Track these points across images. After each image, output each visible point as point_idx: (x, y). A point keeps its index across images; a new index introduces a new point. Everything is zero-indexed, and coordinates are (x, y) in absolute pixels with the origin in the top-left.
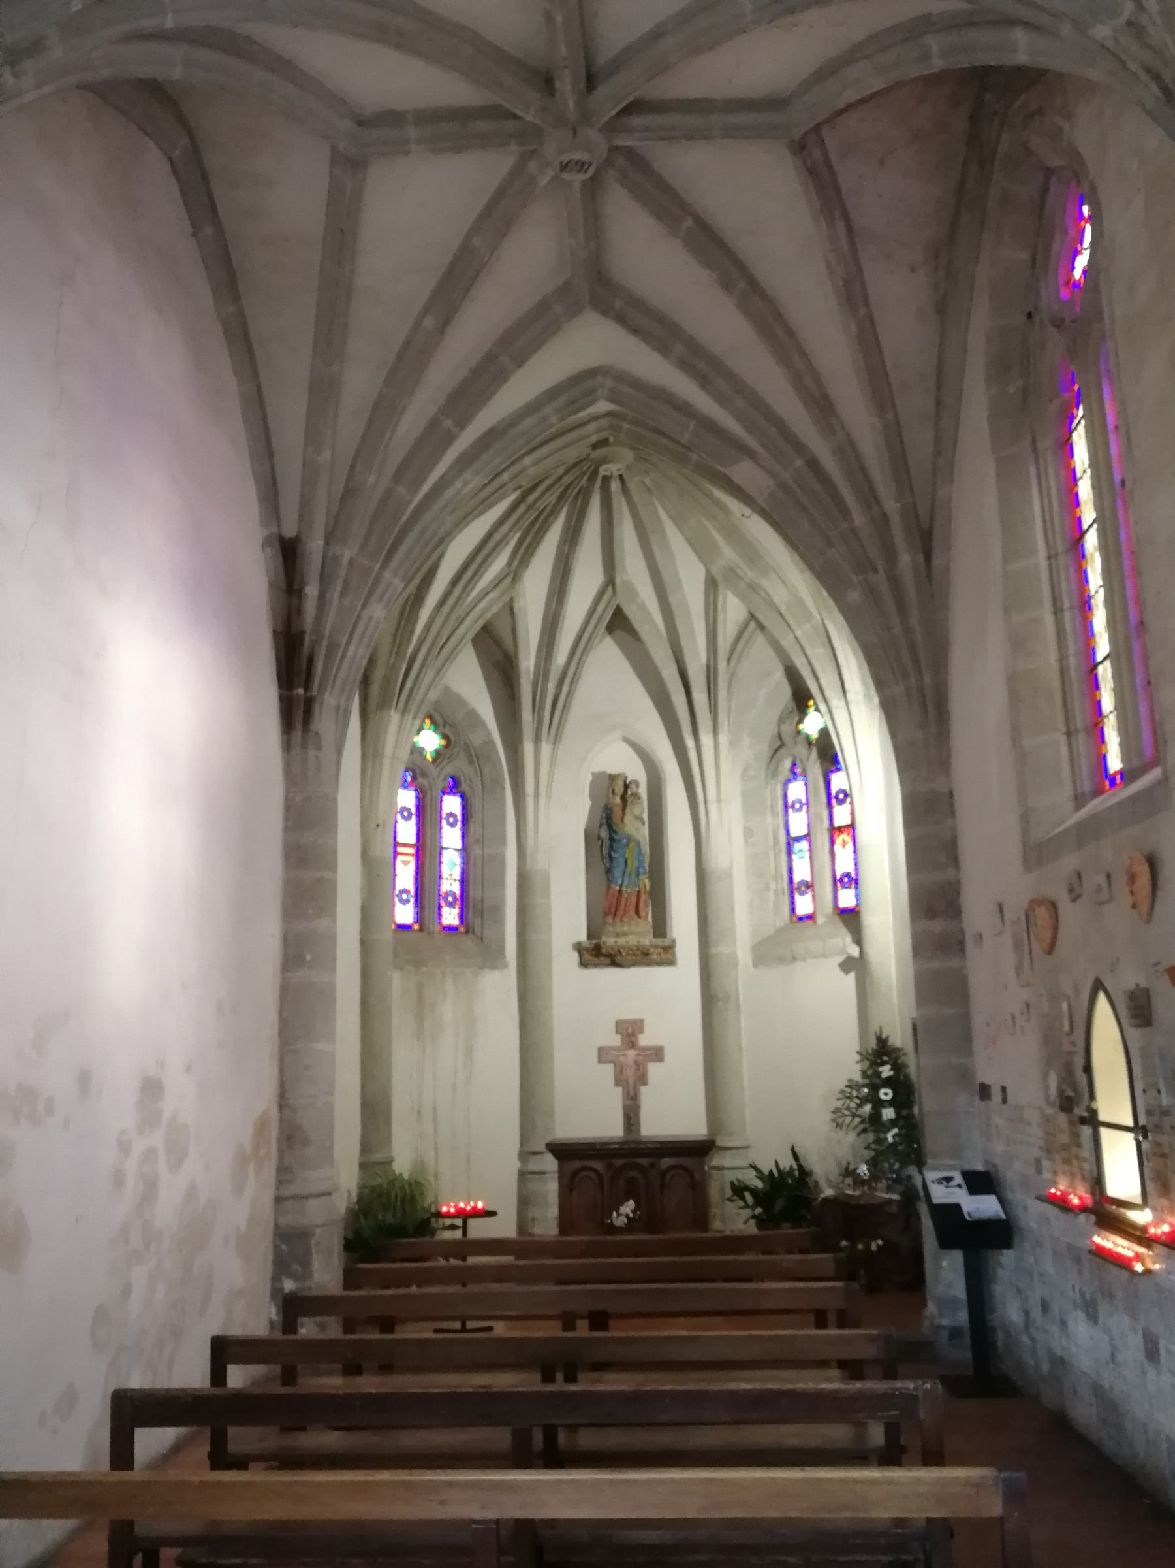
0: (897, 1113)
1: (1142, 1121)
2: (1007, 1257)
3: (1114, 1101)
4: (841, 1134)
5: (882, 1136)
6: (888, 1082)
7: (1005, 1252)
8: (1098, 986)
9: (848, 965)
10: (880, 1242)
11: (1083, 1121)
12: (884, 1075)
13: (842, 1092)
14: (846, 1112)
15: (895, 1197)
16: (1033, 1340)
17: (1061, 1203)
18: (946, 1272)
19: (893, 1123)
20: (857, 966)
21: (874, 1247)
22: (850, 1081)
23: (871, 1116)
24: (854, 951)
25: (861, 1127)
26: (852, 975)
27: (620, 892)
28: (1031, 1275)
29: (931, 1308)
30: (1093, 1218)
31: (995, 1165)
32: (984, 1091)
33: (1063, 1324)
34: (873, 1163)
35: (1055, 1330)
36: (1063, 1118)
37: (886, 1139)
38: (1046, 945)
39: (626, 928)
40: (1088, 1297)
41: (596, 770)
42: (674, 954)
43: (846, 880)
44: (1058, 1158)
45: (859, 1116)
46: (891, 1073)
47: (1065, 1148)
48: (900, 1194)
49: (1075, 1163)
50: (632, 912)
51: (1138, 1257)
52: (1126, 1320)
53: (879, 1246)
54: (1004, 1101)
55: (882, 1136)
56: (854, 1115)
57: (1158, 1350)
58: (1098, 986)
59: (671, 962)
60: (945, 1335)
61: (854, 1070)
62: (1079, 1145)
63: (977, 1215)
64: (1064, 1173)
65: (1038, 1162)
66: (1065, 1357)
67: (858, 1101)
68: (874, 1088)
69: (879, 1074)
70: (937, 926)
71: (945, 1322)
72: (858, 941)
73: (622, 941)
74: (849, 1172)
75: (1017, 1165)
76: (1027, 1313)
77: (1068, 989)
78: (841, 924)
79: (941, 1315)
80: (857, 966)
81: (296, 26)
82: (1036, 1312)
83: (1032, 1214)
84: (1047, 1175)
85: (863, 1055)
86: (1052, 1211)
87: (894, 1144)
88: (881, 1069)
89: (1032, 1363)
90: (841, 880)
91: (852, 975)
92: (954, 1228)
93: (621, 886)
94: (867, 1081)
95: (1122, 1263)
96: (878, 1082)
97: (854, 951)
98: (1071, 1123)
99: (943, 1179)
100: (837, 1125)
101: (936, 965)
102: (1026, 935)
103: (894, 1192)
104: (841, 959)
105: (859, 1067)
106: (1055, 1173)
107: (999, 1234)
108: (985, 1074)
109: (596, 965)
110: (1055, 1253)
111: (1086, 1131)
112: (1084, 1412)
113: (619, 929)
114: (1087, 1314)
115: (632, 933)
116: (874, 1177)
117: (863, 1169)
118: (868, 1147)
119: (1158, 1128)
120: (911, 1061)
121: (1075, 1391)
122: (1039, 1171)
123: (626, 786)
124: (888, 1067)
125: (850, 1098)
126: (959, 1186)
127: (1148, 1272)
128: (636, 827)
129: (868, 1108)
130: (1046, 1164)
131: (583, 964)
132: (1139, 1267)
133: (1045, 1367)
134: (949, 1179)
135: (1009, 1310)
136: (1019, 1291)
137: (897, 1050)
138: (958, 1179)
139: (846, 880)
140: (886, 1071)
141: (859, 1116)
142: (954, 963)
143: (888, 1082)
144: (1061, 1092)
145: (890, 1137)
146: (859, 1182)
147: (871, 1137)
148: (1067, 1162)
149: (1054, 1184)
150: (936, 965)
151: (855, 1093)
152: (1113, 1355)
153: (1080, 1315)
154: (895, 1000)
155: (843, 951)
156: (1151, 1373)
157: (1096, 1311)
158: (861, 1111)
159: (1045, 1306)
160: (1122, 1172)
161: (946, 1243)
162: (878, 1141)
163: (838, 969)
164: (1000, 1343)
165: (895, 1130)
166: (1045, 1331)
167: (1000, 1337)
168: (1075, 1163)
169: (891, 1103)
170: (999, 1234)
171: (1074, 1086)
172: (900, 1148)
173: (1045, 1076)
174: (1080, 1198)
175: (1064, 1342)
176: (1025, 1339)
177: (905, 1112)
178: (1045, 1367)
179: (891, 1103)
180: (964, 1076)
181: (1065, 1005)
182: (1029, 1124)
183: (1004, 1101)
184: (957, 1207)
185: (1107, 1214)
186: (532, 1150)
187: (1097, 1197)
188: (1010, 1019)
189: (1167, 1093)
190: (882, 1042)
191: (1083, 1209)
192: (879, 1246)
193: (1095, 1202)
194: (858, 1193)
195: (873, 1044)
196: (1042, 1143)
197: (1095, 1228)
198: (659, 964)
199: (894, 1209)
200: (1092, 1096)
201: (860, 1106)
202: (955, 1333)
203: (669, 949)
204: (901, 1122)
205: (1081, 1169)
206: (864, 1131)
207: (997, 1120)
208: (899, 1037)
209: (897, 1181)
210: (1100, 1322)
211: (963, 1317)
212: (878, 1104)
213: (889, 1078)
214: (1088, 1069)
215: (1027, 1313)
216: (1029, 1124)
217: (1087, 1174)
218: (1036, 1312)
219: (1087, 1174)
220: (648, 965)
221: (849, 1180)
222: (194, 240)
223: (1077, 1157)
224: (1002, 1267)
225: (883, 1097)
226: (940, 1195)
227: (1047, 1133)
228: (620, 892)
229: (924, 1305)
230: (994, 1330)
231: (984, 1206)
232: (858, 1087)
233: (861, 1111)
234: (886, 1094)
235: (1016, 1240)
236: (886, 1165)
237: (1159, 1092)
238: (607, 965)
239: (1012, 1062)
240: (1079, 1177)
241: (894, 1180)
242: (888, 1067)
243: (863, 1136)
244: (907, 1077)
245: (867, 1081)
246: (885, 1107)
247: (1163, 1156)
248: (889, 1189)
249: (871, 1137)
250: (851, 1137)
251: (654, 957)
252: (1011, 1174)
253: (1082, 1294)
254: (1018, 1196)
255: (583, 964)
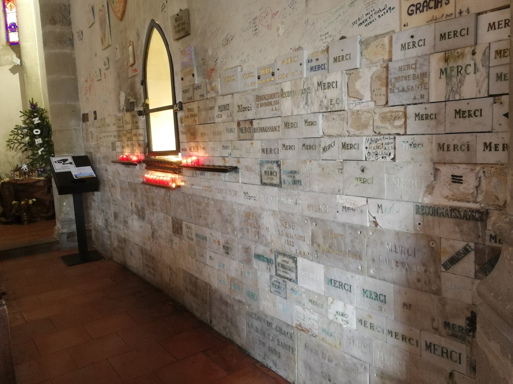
0: (43, 140)
1: (179, 99)
2: (97, 195)
3: (160, 92)
4: (13, 153)
5: (35, 152)
6: (38, 126)
7: (96, 193)
8: (153, 25)
9: (14, 70)
10: (34, 200)
11: (140, 113)
12: (35, 123)
13: (12, 131)
14: (16, 141)
15: (42, 178)
16: (110, 232)
17: (128, 163)
18: (65, 206)
19: (41, 145)
20: (19, 69)
21: (30, 202)
22: (16, 126)
23: (28, 143)
24: (18, 62)
25: (24, 149)
26: (17, 75)
28: (109, 202)
29: (58, 225)
30: (144, 165)
31: (90, 153)
32: (85, 118)
33: (126, 222)
34: (31, 165)
35: (121, 226)
36: (128, 116)
37: (38, 153)
38: (119, 15)
40: (139, 207)
43: (13, 27)
44: (124, 139)
45: (23, 143)
46: (39, 121)
47: (130, 131)
48: (45, 177)
49: (134, 138)
51: (173, 181)
52: (162, 215)
53: (33, 202)
54: (95, 118)
55: (35, 152)
56: (21, 143)
57: (181, 228)
58: (153, 25)
60: (65, 237)
61: (19, 121)
62: (137, 128)
63: (80, 176)
64: (128, 146)
65: (113, 144)
66: (126, 237)
67: (22, 136)
68: (31, 129)
69: (33, 123)
70: (58, 29)
71: (65, 231)
72: (19, 57)
74: (18, 169)
75: (103, 150)
76: (106, 220)
77: (132, 37)
78: (11, 50)
79: (62, 228)
80: (19, 69)
82: (111, 219)
83: (112, 172)
84: (119, 150)
85: (24, 113)
86: (120, 168)
87: (42, 155)
88: (34, 120)
89: (109, 243)
90: (10, 27)
91: (17, 75)
92: (69, 184)
94: (27, 126)
95: (163, 185)
96: (33, 126)
97: (18, 62)
98: (133, 116)
99: (62, 160)
100: (10, 148)
101: (57, 51)
102: (107, 15)
103: (42, 177)
104: (11, 66)
105: (23, 118)
106: (123, 147)
107: (93, 184)
108: (85, 108)
110: (122, 188)
111: (142, 118)
112: (135, 262)
114: (139, 216)
116: (31, 171)
117: (25, 167)
118: (28, 158)
119: (191, 100)
120: (49, 115)
121: (131, 253)
122: (114, 149)
124: (38, 118)
125: (18, 134)
126: (71, 163)
127: (178, 187)
129: (27, 139)
130: (118, 144)
132: (174, 185)
133: (116, 244)
134: (65, 161)
135: (97, 219)
136: (103, 211)
137: (43, 110)
138: (70, 160)
139: (13, 27)
140: (36, 121)
141: (23, 143)
142: (67, 51)
143: (38, 126)
144: (127, 100)
145: (40, 152)
146: (23, 173)
147: (30, 153)
148: (130, 139)
149: (122, 153)
150: (57, 51)
151: (20, 132)
152: (153, 233)
153: (135, 217)
154: (41, 87)
155: (12, 62)
156: (176, 240)
157: (144, 213)
158: (23, 140)
159: (116, 216)
160: (163, 133)
161: (62, 191)
162: (34, 155)
163: (10, 72)
164: (93, 237)
165: (43, 149)
166: (116, 227)
167: (93, 233)
168: (134, 138)
169: (40, 136)
170: (93, 184)
171: (135, 96)
172: (45, 157)
173: (119, 95)
174: (137, 156)
175: (126, 231)
176: (106, 233)
177: (46, 139)
178: (116, 244)
179: (40, 136)
180: (74, 111)
181: (130, 48)
182: (109, 126)
183: (95, 118)
184: (70, 173)
185: (153, 161)
186: (384, 282)
187: (147, 154)
188: (98, 72)
189: (198, 76)
190: (34, 106)
191: (139, 162)
192: (33, 202)
193: (146, 157)
194: (22, 178)
195: (29, 108)
196: (115, 134)
197: (146, 171)
199: (41, 184)
200: (146, 97)
201: (23, 138)
202: (70, 235)
204: (45, 145)
205: (138, 141)
206: (26, 150)
207: (91, 129)
208: (43, 103)
209: (44, 171)
210: (146, 219)
211: (74, 227)
212: (33, 137)
213: (38, 124)
214: (144, 83)
215: (106, 220)
216: (109, 126)
217: (141, 143)
218: (111, 219)
219: (141, 143)
221: (17, 173)
223: (136, 135)
224: (94, 201)
225: (35, 133)
226: (59, 168)
227: (119, 127)
229: (55, 224)
230: (90, 231)
231: (86, 171)
232: (22, 129)
233: (23, 140)
234: (37, 132)
235: (101, 186)
236: (38, 165)
237: (193, 75)
239: (101, 97)
240: (137, 145)
241: (42, 172)
242: (38, 118)
243: (25, 152)
244: (48, 123)
245: (27, 126)
246: (37, 138)
247: (194, 116)
248: (39, 176)
249: (30, 153)
250: (20, 154)
252: (98, 156)
253: (136, 206)
254: (102, 165)
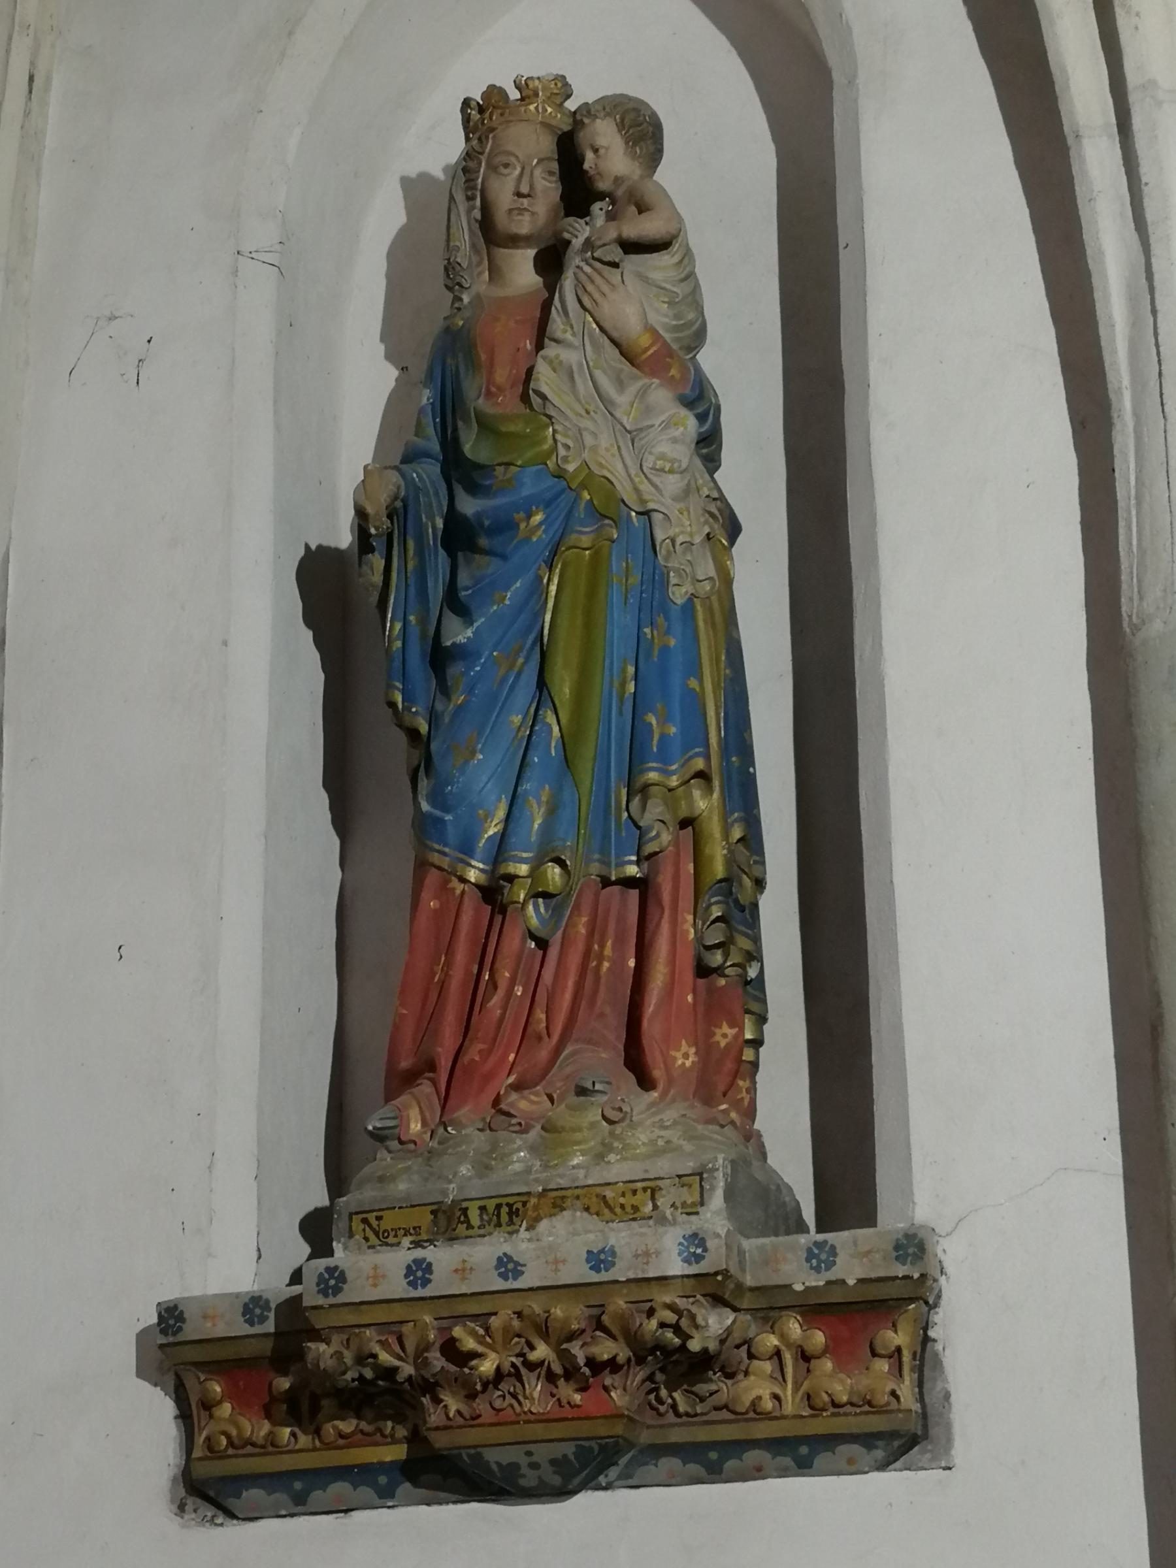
27: (493, 893)
39: (519, 1162)
41: (413, 172)
42: (924, 1358)
50: (600, 1058)
59: (904, 1436)
73: (464, 1264)
81: (1156, 137)
93: (501, 849)
109: (299, 1492)
113: (462, 1180)
115: (557, 1201)
123: (569, 151)
128: (671, 437)
131: (210, 1488)
198: (800, 1452)
203: (887, 1310)
220: (712, 1462)
222: (932, 1333)
228: (493, 893)
238: (384, 1485)
251: (757, 1387)
255: (210, 1488)
